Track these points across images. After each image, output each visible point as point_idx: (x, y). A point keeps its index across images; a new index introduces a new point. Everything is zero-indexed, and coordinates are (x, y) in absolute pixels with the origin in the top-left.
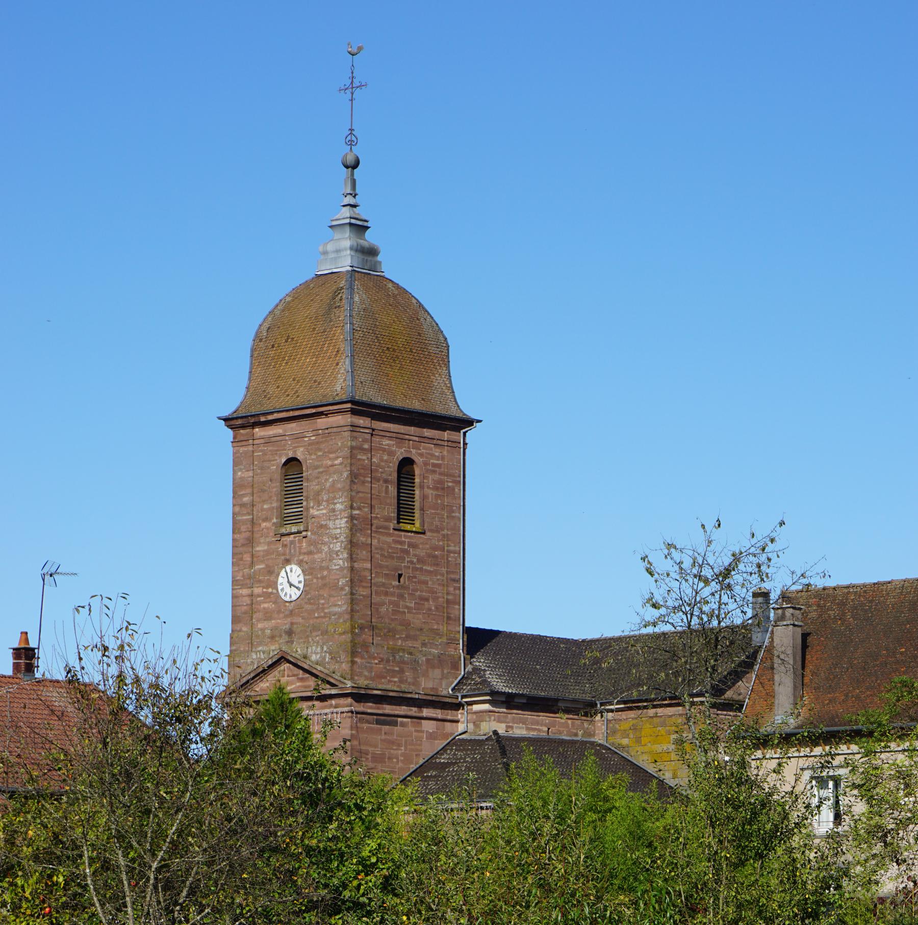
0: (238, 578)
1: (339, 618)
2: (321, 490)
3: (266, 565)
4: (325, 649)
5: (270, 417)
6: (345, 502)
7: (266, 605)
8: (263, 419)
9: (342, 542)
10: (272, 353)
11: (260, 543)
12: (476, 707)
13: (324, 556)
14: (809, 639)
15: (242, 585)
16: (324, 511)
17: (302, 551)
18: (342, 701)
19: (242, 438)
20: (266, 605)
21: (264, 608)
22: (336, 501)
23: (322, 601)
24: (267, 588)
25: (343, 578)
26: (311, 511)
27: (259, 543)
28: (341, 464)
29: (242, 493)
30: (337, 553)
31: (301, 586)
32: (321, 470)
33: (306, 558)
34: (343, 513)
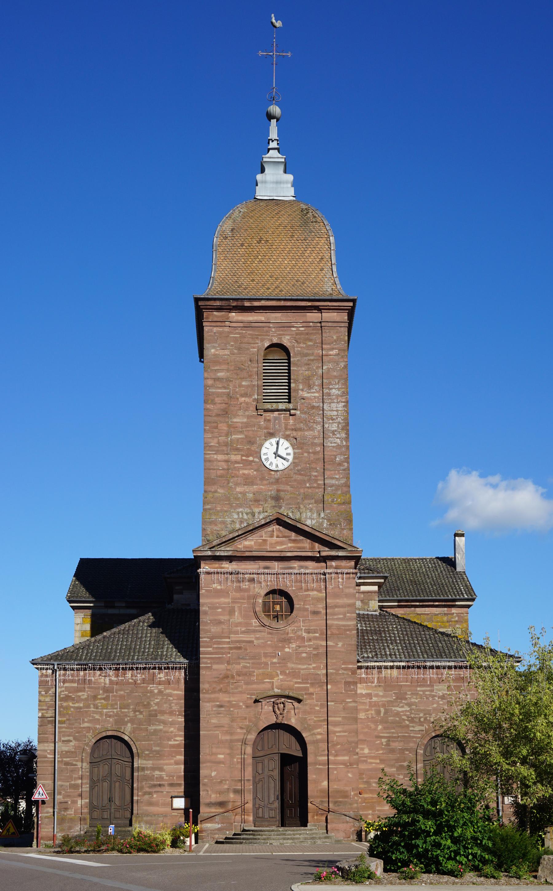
0: (212, 444)
1: (337, 490)
2: (313, 376)
3: (246, 436)
4: (322, 515)
5: (256, 304)
6: (342, 388)
7: (246, 472)
8: (247, 304)
9: (339, 423)
11: (238, 415)
13: (316, 433)
15: (218, 451)
16: (316, 395)
17: (289, 427)
18: (344, 563)
19: (215, 319)
20: (246, 472)
21: (244, 474)
22: (331, 387)
24: (248, 456)
25: (341, 454)
26: (301, 393)
27: (236, 416)
29: (216, 368)
30: (333, 432)
31: (290, 458)
32: (312, 358)
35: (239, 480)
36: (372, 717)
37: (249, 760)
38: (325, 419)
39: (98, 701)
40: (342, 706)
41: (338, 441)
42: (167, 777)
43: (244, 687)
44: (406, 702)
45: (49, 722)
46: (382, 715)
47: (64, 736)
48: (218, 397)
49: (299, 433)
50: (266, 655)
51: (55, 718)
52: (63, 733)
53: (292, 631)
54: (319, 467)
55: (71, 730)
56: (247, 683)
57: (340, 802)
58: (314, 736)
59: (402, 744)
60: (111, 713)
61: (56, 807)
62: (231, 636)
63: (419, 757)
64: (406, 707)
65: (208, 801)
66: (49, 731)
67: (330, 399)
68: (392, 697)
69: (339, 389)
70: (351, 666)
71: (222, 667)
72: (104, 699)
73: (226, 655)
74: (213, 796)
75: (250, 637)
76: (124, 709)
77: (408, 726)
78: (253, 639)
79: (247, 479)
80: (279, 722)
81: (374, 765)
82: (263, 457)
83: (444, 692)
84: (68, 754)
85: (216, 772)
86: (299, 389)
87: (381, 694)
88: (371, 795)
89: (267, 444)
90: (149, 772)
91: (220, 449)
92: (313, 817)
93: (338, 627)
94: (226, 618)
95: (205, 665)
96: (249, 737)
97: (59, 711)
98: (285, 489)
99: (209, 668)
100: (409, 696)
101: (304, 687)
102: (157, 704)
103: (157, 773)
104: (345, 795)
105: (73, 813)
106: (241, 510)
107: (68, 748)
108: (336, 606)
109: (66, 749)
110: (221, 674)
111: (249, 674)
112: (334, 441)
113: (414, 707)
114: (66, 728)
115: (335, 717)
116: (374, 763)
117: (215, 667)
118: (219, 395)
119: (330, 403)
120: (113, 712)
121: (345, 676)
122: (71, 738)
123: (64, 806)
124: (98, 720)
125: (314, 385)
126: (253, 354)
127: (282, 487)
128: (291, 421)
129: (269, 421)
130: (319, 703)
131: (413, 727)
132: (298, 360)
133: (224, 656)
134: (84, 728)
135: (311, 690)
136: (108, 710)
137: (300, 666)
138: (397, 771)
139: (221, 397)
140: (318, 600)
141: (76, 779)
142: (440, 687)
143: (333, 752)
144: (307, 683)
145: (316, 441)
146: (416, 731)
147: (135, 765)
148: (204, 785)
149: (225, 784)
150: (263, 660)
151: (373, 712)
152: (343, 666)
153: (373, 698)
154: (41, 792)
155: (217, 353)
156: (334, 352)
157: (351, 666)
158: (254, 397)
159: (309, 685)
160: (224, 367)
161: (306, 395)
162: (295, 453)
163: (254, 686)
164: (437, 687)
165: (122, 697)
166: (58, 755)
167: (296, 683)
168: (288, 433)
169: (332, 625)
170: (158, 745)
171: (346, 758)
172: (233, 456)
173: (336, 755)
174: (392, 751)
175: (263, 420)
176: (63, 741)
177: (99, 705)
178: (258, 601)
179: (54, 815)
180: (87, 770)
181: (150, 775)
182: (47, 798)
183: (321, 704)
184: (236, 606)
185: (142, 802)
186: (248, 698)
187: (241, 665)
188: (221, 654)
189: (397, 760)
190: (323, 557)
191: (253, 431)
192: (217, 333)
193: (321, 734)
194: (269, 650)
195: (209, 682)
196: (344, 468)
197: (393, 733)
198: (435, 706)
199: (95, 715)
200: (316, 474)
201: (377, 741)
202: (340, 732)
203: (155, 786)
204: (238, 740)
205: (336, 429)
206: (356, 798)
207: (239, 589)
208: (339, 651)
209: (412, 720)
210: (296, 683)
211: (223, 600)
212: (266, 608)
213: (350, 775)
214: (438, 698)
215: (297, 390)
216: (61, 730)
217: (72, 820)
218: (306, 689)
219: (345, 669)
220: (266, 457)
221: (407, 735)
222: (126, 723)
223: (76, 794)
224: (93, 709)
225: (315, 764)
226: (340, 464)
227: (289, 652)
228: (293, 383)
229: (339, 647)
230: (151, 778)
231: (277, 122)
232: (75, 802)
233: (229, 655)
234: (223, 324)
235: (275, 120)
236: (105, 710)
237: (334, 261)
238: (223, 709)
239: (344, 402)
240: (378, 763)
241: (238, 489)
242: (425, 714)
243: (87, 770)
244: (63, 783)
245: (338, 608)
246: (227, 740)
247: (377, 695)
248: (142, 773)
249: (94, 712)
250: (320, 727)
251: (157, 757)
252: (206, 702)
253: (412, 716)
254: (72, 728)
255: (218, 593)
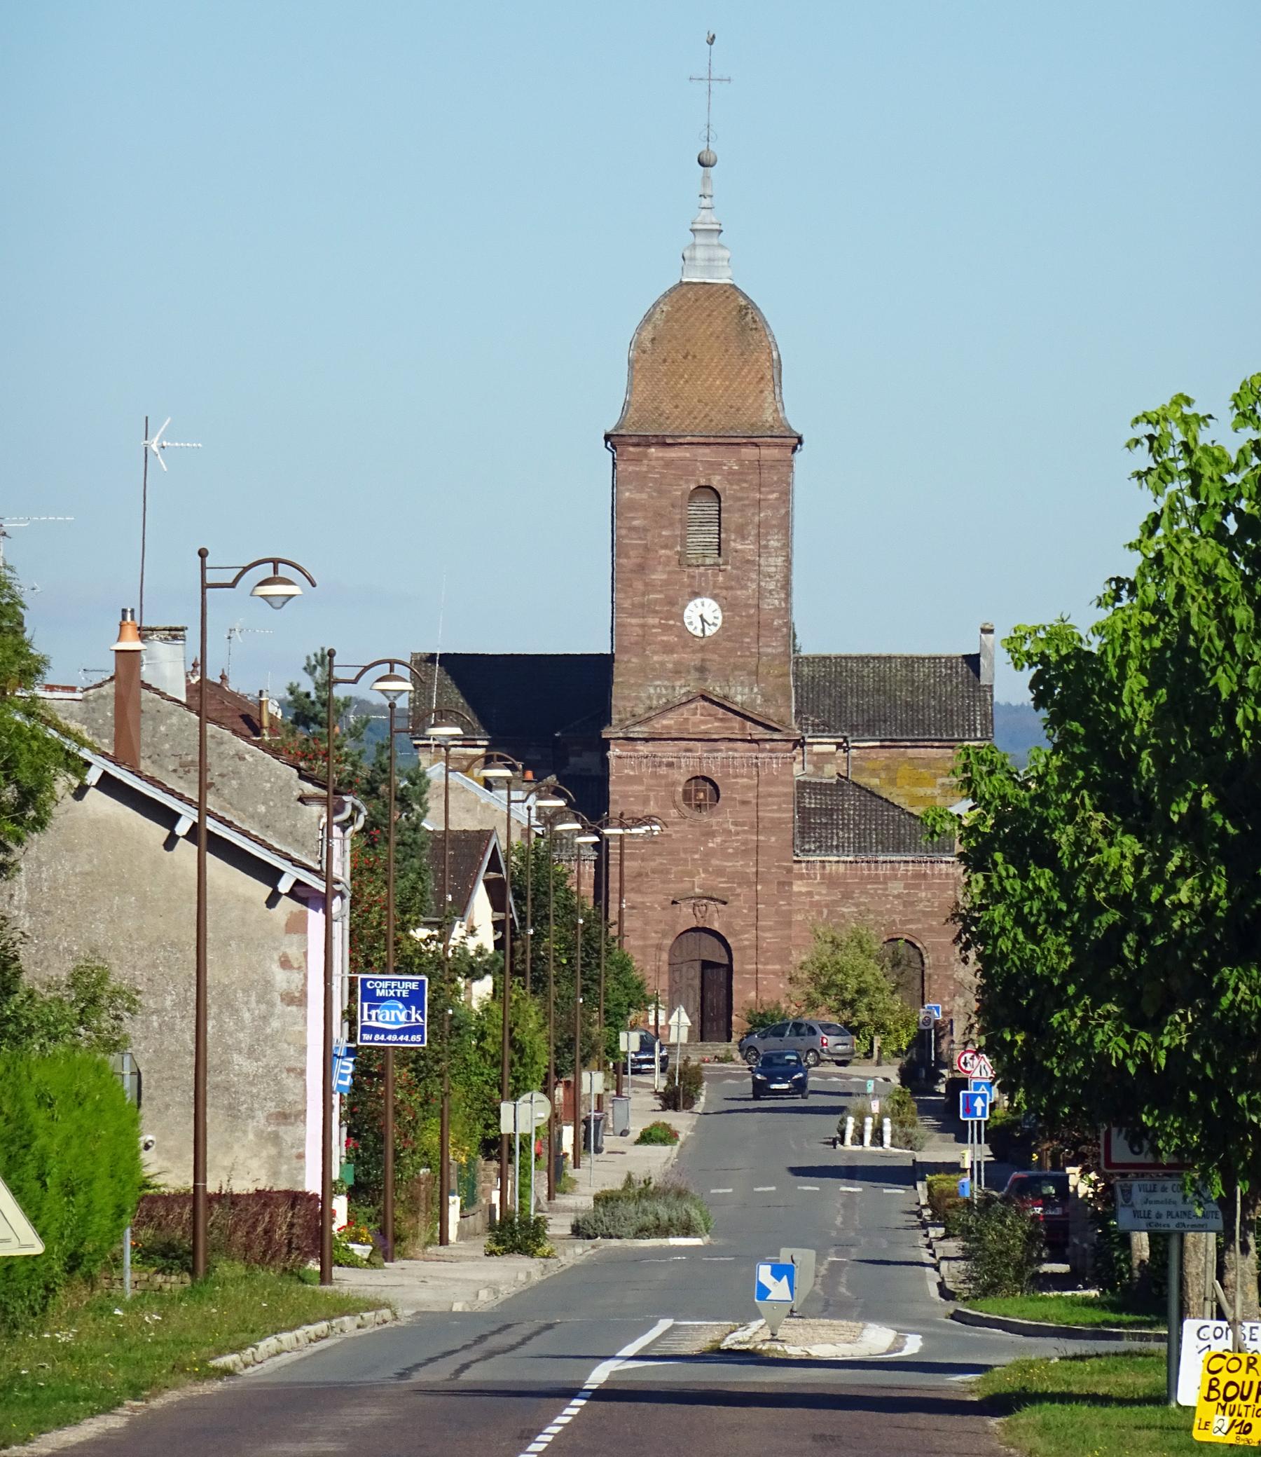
2: (747, 524)
4: (756, 690)
10: (663, 368)
12: (816, 748)
14: (8, 563)
23: (747, 640)
24: (667, 619)
26: (733, 544)
27: (654, 571)
28: (776, 499)
32: (746, 502)
33: (724, 593)
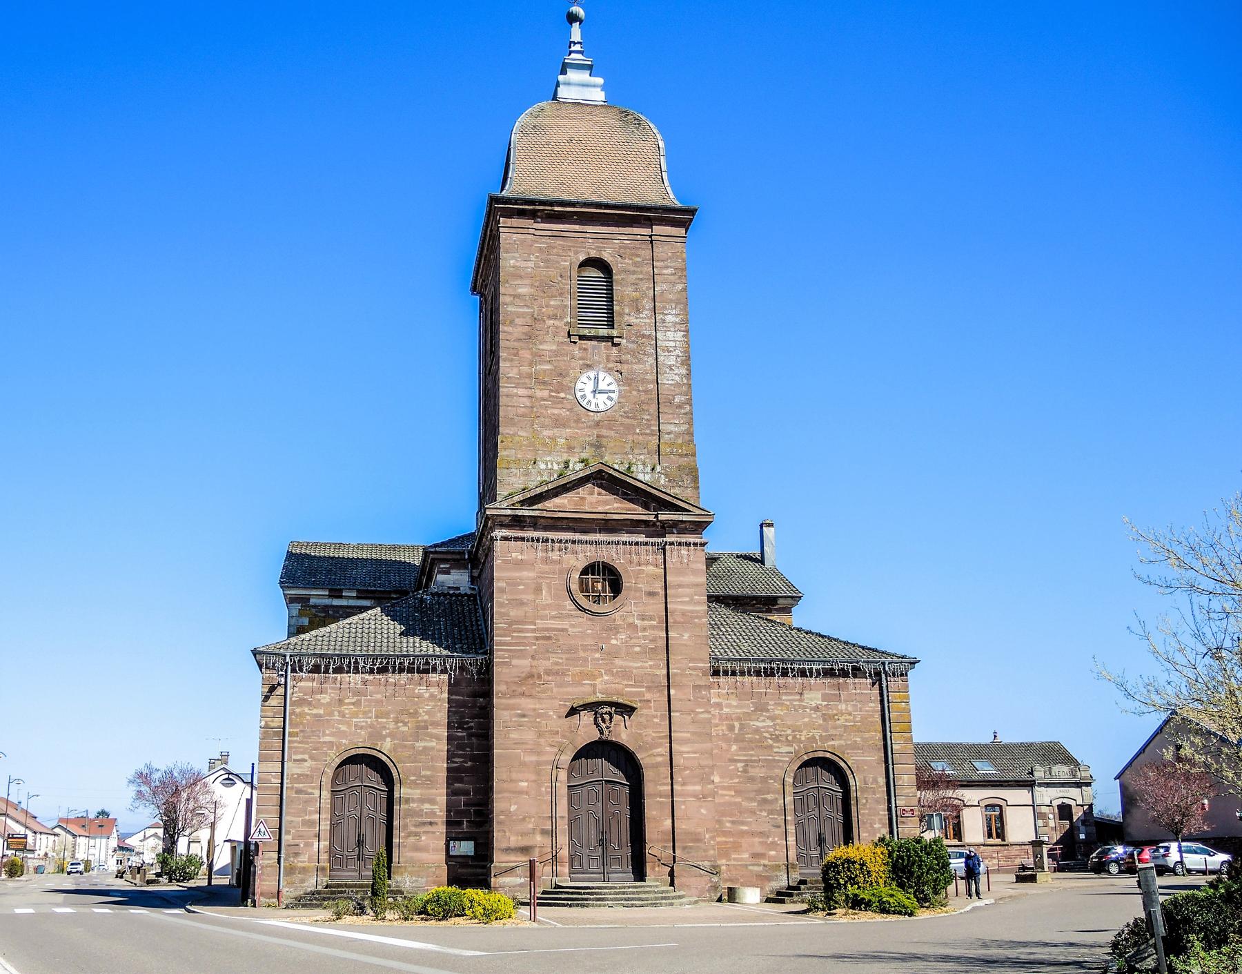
2: (643, 298)
4: (658, 468)
7: (556, 411)
20: (556, 411)
21: (554, 415)
25: (681, 394)
29: (515, 283)
30: (670, 367)
32: (641, 276)
34: (678, 327)
35: (548, 421)
36: (723, 735)
37: (563, 791)
38: (658, 350)
39: (345, 707)
40: (690, 718)
41: (677, 378)
42: (441, 812)
43: (555, 690)
44: (767, 715)
45: (276, 734)
46: (736, 732)
47: (296, 753)
48: (518, 317)
49: (625, 366)
50: (585, 648)
51: (284, 728)
52: (294, 750)
53: (621, 617)
54: (653, 409)
55: (307, 746)
56: (559, 686)
57: (691, 848)
58: (653, 758)
59: (764, 770)
60: (364, 724)
61: (283, 852)
62: (537, 621)
63: (787, 788)
64: (767, 721)
65: (504, 845)
66: (275, 747)
67: (665, 326)
68: (750, 707)
69: (676, 315)
70: (702, 665)
71: (525, 663)
72: (353, 704)
73: (531, 646)
74: (513, 838)
75: (564, 624)
76: (382, 718)
77: (771, 747)
78: (567, 627)
79: (557, 420)
80: (604, 737)
81: (727, 797)
82: (579, 394)
83: (818, 702)
84: (300, 778)
85: (516, 806)
86: (624, 313)
87: (735, 703)
88: (724, 839)
89: (584, 378)
90: (415, 805)
91: (521, 381)
92: (653, 868)
93: (684, 614)
94: (531, 597)
95: (501, 660)
96: (563, 758)
97: (290, 719)
98: (608, 434)
99: (508, 664)
100: (772, 707)
101: (636, 691)
102: (427, 713)
103: (427, 806)
104: (697, 839)
105: (306, 860)
106: (549, 458)
107: (302, 770)
108: (680, 586)
109: (299, 771)
110: (522, 672)
111: (562, 673)
112: (668, 379)
113: (779, 721)
114: (300, 742)
115: (681, 732)
116: (726, 795)
117: (515, 662)
118: (519, 315)
119: (666, 331)
120: (367, 722)
121: (694, 678)
122: (306, 757)
123: (295, 849)
124: (344, 732)
125: (644, 307)
126: (564, 268)
127: (604, 432)
128: (615, 350)
129: (585, 349)
130: (659, 714)
131: (779, 748)
132: (623, 279)
133: (528, 648)
134: (324, 742)
135: (648, 696)
136: (358, 720)
137: (631, 664)
138: (758, 806)
139: (524, 318)
140: (655, 577)
141: (311, 813)
142: (813, 696)
143: (680, 779)
144: (642, 686)
145: (648, 377)
146: (782, 753)
147: (396, 795)
148: (500, 823)
149: (529, 822)
150: (582, 654)
151: (724, 728)
152: (690, 665)
153: (725, 709)
154: (263, 830)
155: (517, 264)
156: (669, 271)
157: (702, 665)
158: (565, 320)
159: (644, 689)
160: (527, 282)
161: (633, 321)
162: (620, 391)
163: (570, 689)
164: (808, 696)
165: (379, 702)
166: (287, 779)
167: (627, 686)
168: (611, 365)
169: (675, 611)
170: (428, 768)
171: (698, 788)
172: (539, 390)
173: (684, 784)
174: (752, 779)
175: (578, 349)
176: (295, 760)
177: (347, 711)
178: (574, 577)
179: (279, 862)
180: (327, 801)
181: (417, 809)
182: (271, 838)
183: (661, 715)
184: (544, 582)
185: (405, 846)
186: (560, 705)
187: (551, 661)
188: (523, 646)
189: (759, 792)
190: (661, 521)
191: (564, 361)
192: (518, 241)
193: (662, 755)
194: (590, 641)
195: (507, 683)
196: (685, 411)
197: (752, 755)
198: (806, 720)
199: (340, 726)
200: (648, 417)
201: (730, 766)
202: (688, 753)
203: (424, 824)
204: (546, 763)
205: (674, 363)
206: (712, 842)
207: (546, 561)
208: (686, 645)
209: (776, 739)
210: (627, 686)
211: (525, 574)
212: (584, 587)
213: (703, 811)
214: (811, 710)
215: (621, 314)
216: (292, 745)
217: (304, 870)
218: (641, 694)
219: (694, 669)
220: (582, 393)
221: (770, 758)
222: (383, 738)
223: (312, 833)
224: (338, 718)
225: (655, 795)
226: (680, 406)
227: (616, 645)
228: (617, 305)
229: (685, 640)
230: (419, 813)
231: (580, 24)
232: (308, 845)
233: (534, 647)
234: (525, 231)
235: (578, 23)
236: (355, 720)
237: (664, 168)
238: (526, 719)
239: (683, 331)
240: (733, 796)
241: (546, 433)
242: (793, 731)
243: (327, 801)
244: (293, 819)
245: (683, 588)
246: (531, 762)
247: (729, 706)
248: (406, 807)
249: (339, 722)
250: (660, 745)
251: (428, 784)
252: (503, 709)
253: (777, 733)
254: (307, 743)
255: (520, 564)
